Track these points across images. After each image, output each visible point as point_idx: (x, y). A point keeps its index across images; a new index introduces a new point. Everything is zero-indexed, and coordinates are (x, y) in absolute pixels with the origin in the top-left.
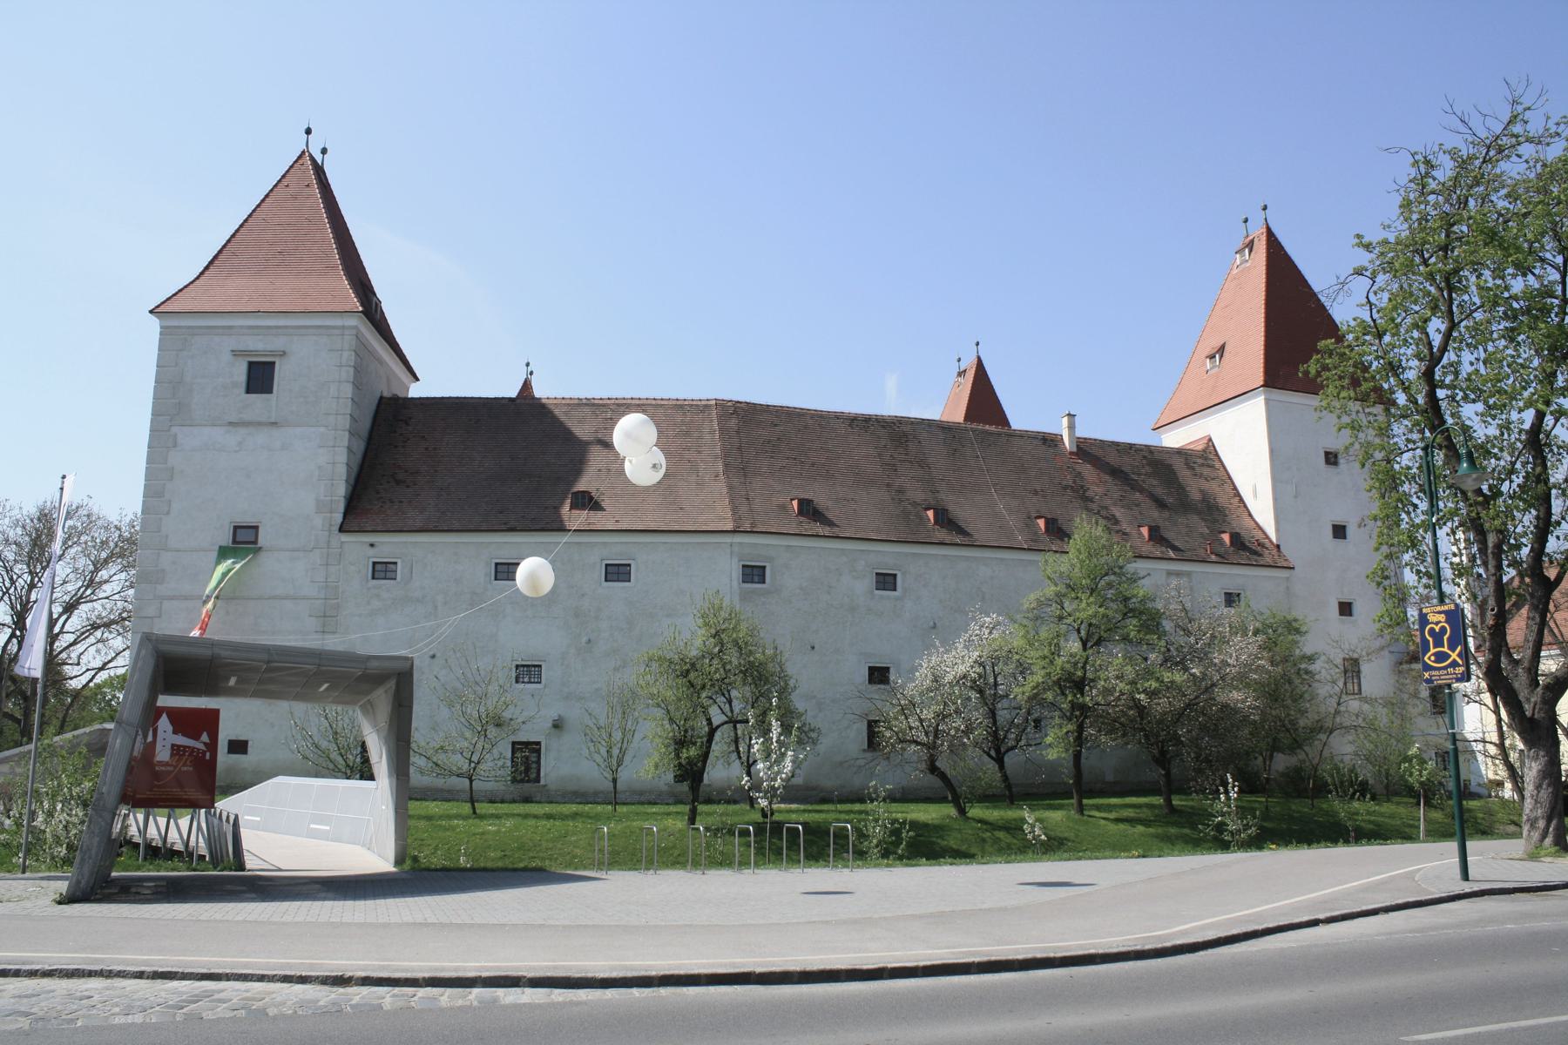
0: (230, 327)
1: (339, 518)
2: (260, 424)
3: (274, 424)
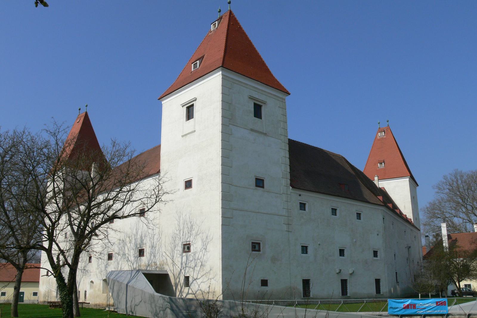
1: (289, 182)
3: (265, 134)
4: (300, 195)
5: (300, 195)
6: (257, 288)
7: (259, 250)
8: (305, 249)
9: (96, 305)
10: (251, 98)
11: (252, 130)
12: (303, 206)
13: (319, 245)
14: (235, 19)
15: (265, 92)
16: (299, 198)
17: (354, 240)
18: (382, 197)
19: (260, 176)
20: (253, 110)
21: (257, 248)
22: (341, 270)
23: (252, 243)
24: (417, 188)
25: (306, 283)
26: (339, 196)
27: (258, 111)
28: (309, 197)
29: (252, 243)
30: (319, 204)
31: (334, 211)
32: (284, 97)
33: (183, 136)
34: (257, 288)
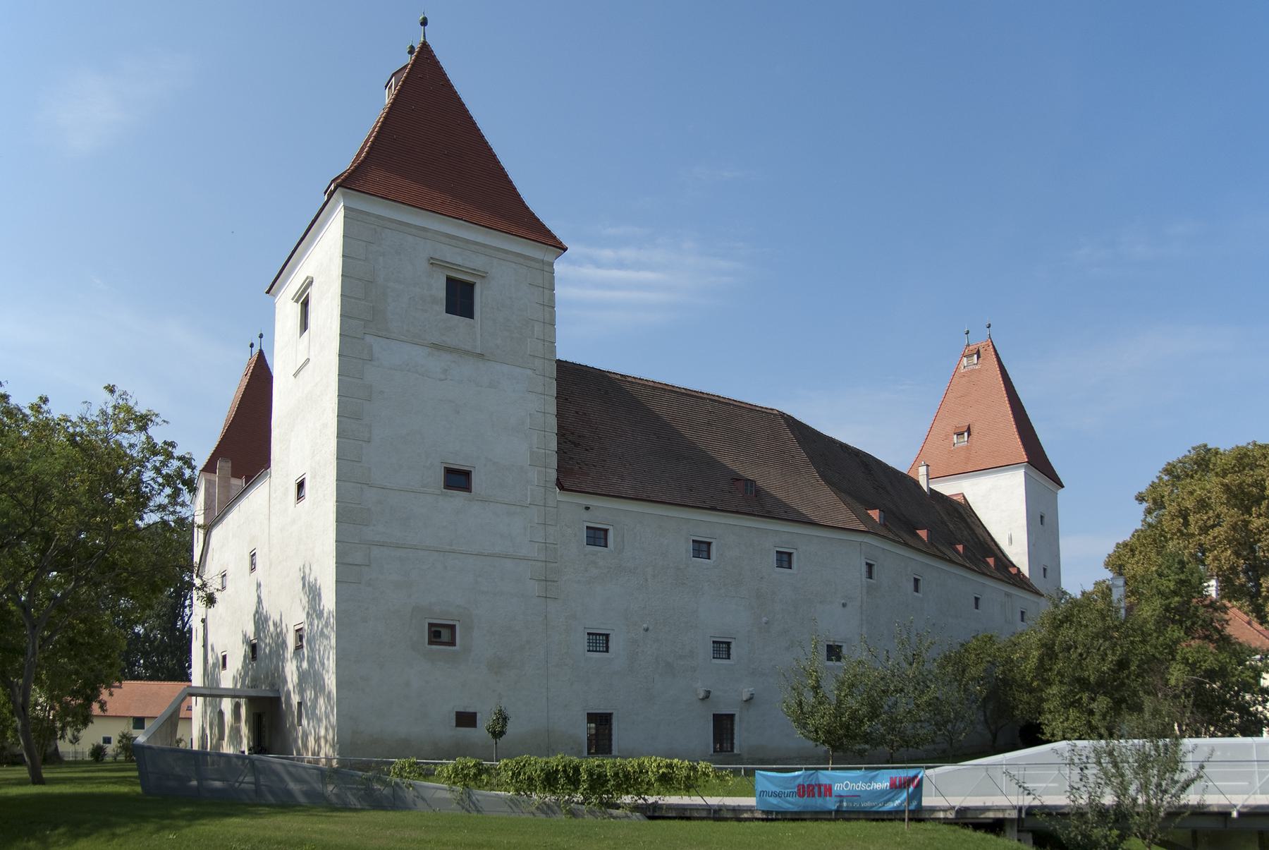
0: (425, 229)
1: (553, 475)
2: (467, 353)
3: (481, 356)
4: (587, 508)
5: (587, 508)
6: (449, 732)
7: (453, 643)
8: (599, 641)
9: (1219, 806)
10: (434, 263)
11: (437, 347)
12: (597, 536)
13: (647, 630)
14: (436, 64)
15: (484, 246)
16: (586, 515)
17: (764, 619)
18: (230, 464)
19: (459, 463)
20: (443, 294)
21: (445, 635)
22: (709, 692)
23: (431, 625)
24: (1061, 492)
25: (601, 722)
26: (713, 509)
27: (460, 297)
28: (605, 510)
29: (431, 625)
30: (652, 532)
31: (702, 549)
32: (548, 258)
33: (295, 375)
34: (449, 732)
